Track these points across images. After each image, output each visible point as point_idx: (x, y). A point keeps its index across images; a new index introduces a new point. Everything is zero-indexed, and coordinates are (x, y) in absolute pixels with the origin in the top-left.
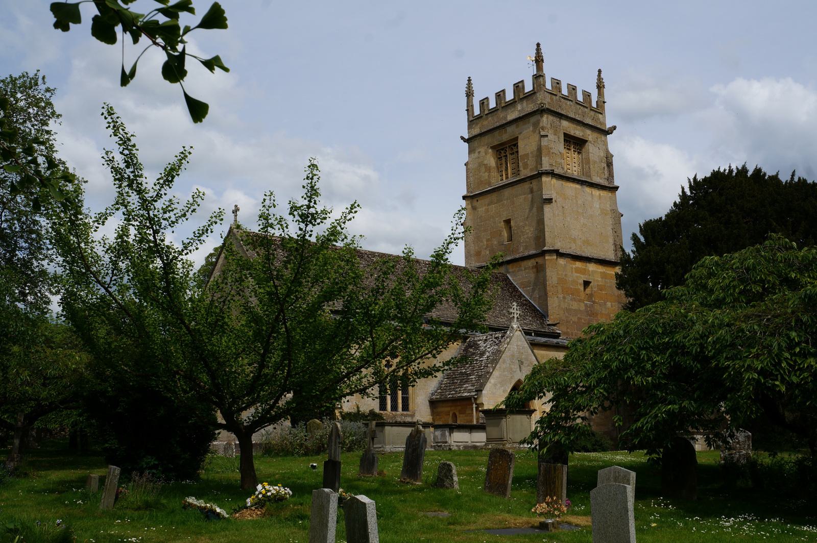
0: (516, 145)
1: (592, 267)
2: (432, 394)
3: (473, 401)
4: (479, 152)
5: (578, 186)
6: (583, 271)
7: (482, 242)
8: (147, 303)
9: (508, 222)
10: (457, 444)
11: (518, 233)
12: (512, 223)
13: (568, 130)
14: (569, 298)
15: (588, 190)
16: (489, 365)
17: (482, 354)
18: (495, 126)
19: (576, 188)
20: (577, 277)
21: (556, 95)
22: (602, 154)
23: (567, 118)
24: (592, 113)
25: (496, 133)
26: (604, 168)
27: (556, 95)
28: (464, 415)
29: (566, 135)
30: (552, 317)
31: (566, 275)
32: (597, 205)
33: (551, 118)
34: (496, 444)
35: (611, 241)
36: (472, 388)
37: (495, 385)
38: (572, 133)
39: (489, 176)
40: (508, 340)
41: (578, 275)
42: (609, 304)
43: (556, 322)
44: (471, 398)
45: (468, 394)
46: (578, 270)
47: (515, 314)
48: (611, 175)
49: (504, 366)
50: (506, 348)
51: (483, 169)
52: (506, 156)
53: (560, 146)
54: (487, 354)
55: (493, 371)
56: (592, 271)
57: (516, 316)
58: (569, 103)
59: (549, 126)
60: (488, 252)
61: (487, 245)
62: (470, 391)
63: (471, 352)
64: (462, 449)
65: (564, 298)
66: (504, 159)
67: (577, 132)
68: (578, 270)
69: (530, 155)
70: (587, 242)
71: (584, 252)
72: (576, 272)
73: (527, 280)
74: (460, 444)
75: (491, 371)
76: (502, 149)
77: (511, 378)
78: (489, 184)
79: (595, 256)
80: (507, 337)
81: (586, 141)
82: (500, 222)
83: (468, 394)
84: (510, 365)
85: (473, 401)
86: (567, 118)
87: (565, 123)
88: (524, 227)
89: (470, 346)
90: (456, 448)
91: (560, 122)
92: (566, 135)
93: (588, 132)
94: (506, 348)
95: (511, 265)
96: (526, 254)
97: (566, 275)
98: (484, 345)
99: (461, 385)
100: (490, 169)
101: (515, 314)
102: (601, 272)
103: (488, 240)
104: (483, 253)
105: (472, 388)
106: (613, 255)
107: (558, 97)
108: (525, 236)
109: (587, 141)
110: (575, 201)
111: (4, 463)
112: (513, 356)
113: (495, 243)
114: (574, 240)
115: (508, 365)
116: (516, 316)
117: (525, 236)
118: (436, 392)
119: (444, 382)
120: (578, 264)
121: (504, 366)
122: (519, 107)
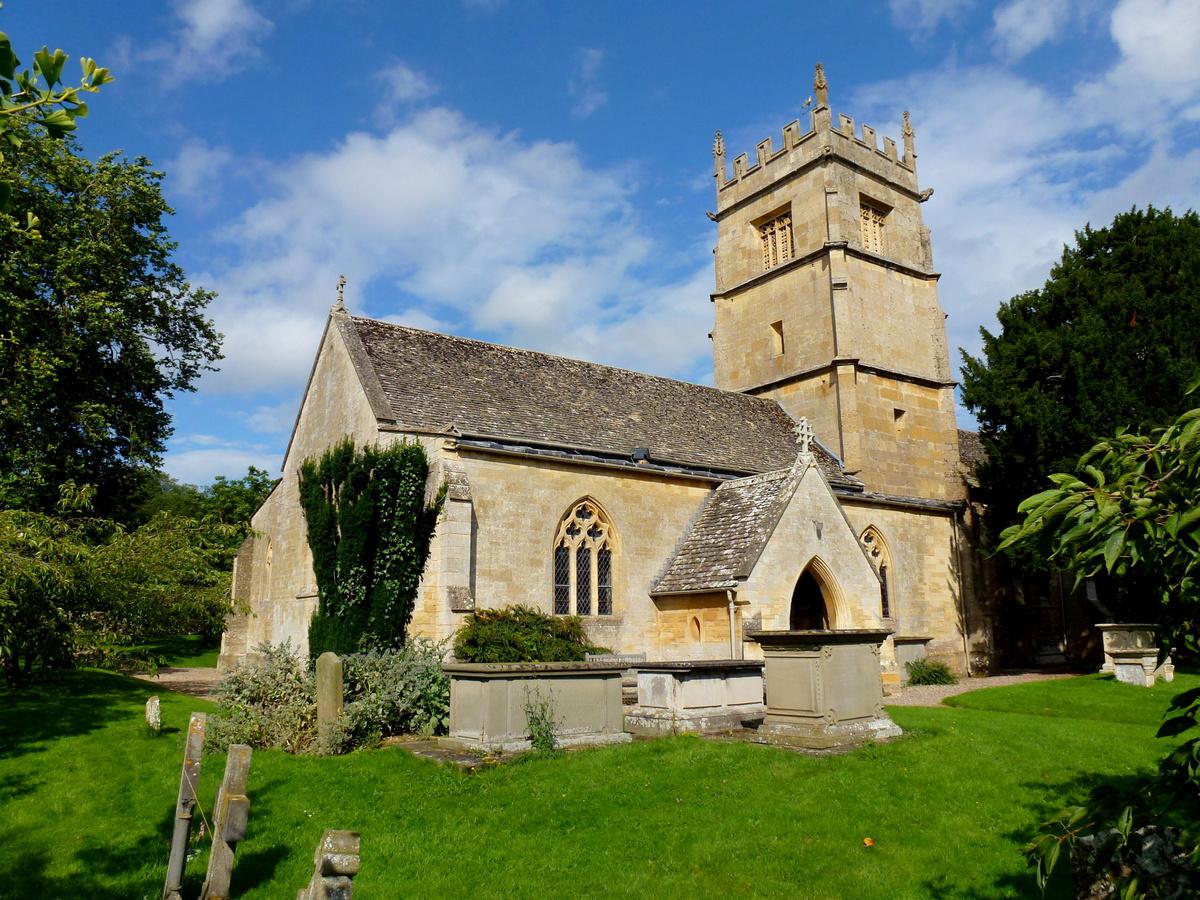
0: (788, 215)
1: (905, 389)
2: (656, 583)
3: (730, 597)
4: (734, 232)
5: (882, 270)
6: (894, 395)
7: (740, 358)
8: (1064, 654)
9: (778, 326)
10: (692, 712)
11: (793, 340)
12: (784, 327)
13: (866, 189)
14: (873, 436)
15: (896, 276)
16: (759, 530)
17: (745, 510)
18: (757, 190)
19: (880, 273)
20: (885, 403)
21: (847, 138)
22: (915, 228)
23: (864, 172)
24: (899, 169)
25: (759, 202)
26: (918, 248)
27: (847, 138)
28: (712, 623)
29: (863, 197)
30: (850, 462)
31: (868, 400)
32: (909, 300)
33: (841, 168)
34: (795, 724)
35: (931, 353)
36: (728, 572)
37: (771, 566)
38: (871, 194)
39: (749, 265)
40: (794, 483)
41: (887, 400)
42: (931, 445)
43: (856, 469)
44: (725, 593)
45: (721, 584)
46: (885, 393)
47: (805, 437)
48: (928, 258)
49: (788, 531)
50: (791, 498)
51: (740, 255)
52: (774, 233)
53: (856, 211)
54: (755, 510)
55: (767, 540)
56: (906, 395)
57: (806, 441)
58: (865, 151)
59: (838, 181)
60: (748, 372)
61: (747, 361)
62: (725, 578)
63: (724, 508)
64: (703, 725)
65: (867, 434)
66: (769, 237)
67: (878, 192)
68: (885, 393)
69: (810, 225)
70: (897, 353)
71: (893, 366)
72: (883, 396)
73: (808, 409)
74: (702, 711)
75: (764, 540)
76: (767, 225)
77: (801, 553)
78: (750, 274)
79: (911, 374)
80: (792, 479)
81: (892, 208)
82: (766, 328)
83: (721, 584)
84: (798, 528)
85: (730, 597)
86: (864, 172)
87: (861, 178)
88: (802, 331)
89: (723, 498)
90: (690, 725)
91: (853, 176)
92: (863, 197)
93: (894, 194)
94: (791, 498)
95: (783, 388)
96: (807, 369)
97: (868, 400)
98: (750, 495)
99: (706, 568)
100: (749, 254)
101: (805, 437)
102: (919, 398)
103: (748, 355)
104: (741, 375)
105: (728, 572)
106: (935, 373)
107: (849, 142)
108: (805, 344)
109: (892, 208)
110: (878, 291)
111: (1174, 497)
112: (803, 513)
113: (759, 357)
114: (879, 349)
115: (795, 530)
116: (806, 441)
117: (805, 344)
118: (662, 579)
119: (678, 562)
120: (886, 384)
121: (788, 531)
122: (792, 157)
